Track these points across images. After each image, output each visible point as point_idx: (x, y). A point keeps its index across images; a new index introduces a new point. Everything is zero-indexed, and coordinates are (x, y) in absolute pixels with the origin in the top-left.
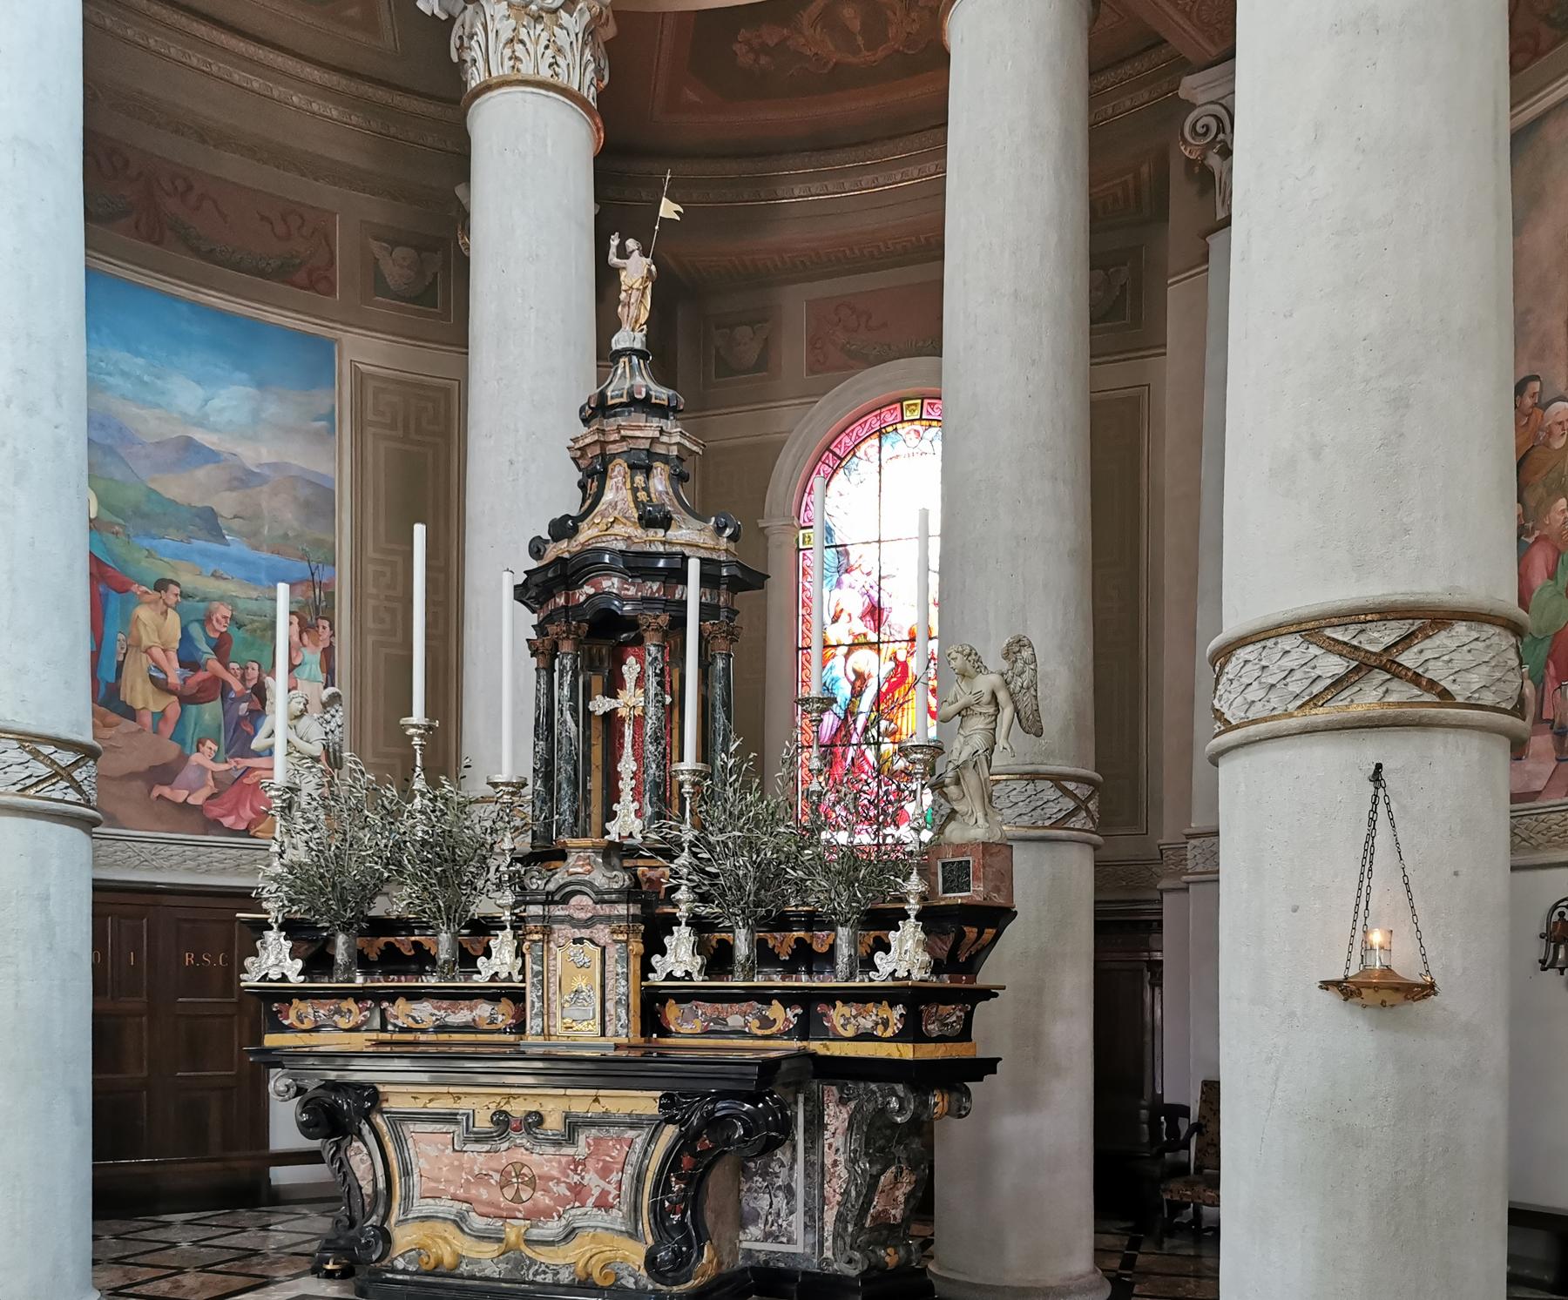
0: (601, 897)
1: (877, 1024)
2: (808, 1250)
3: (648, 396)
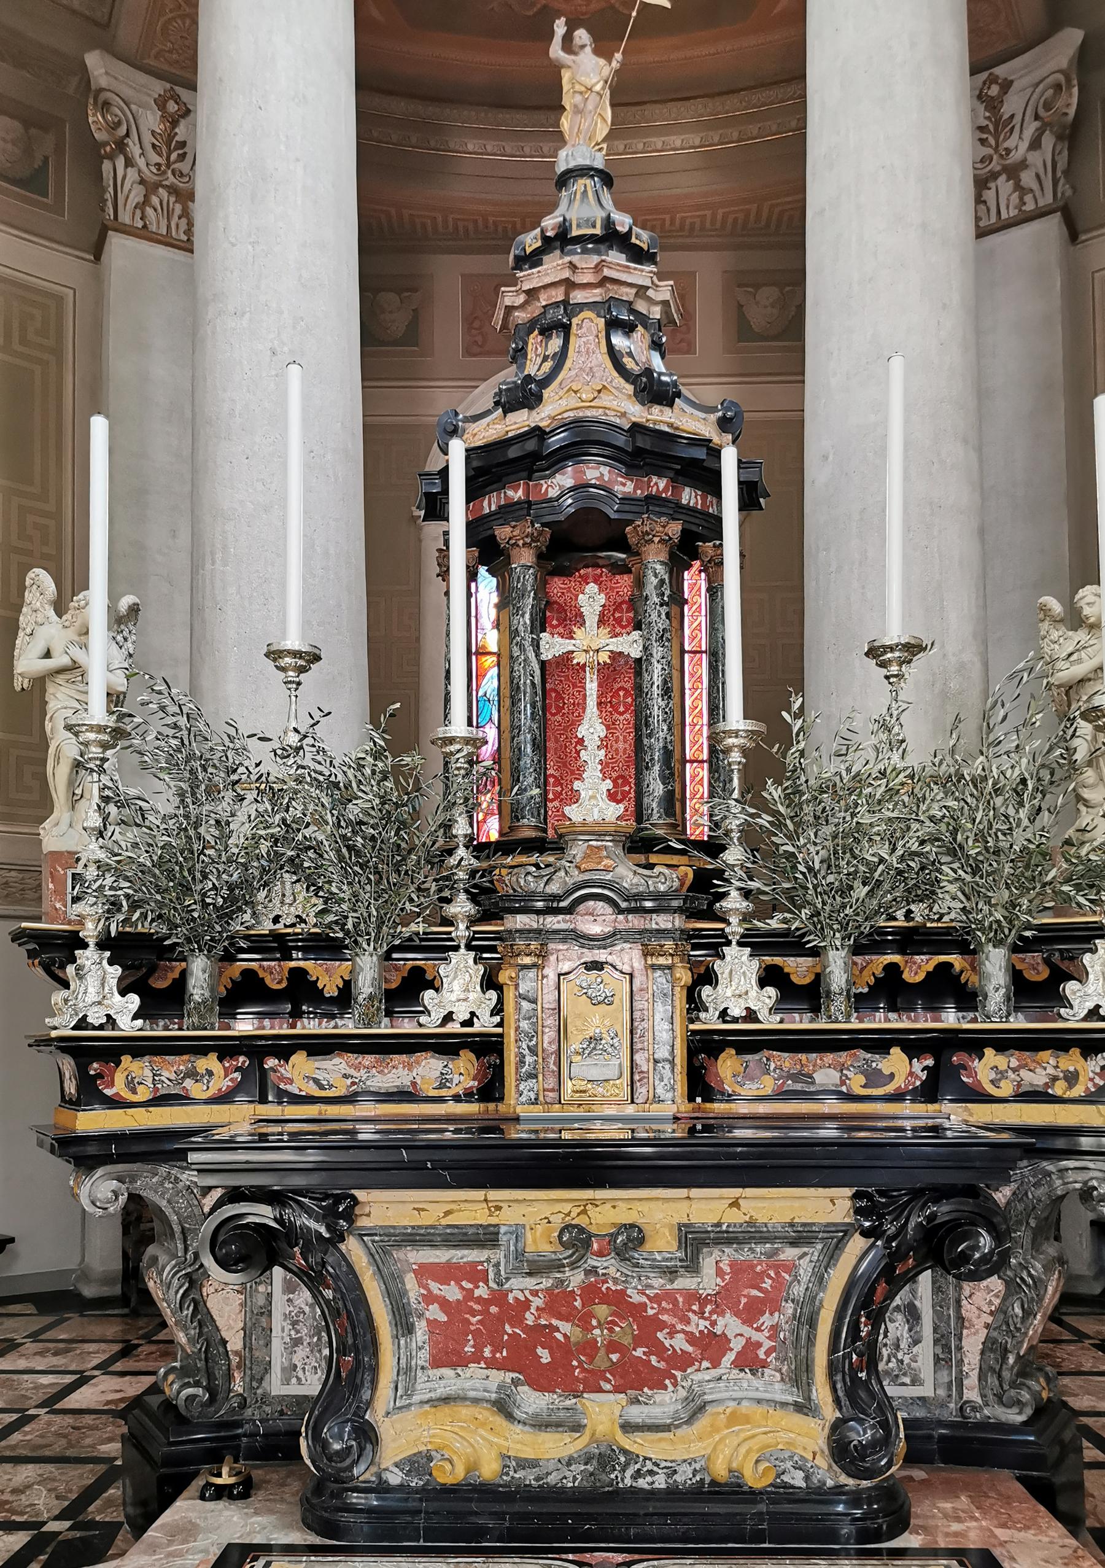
0: (632, 903)
1: (1055, 1079)
2: (942, 1392)
3: (629, 233)
